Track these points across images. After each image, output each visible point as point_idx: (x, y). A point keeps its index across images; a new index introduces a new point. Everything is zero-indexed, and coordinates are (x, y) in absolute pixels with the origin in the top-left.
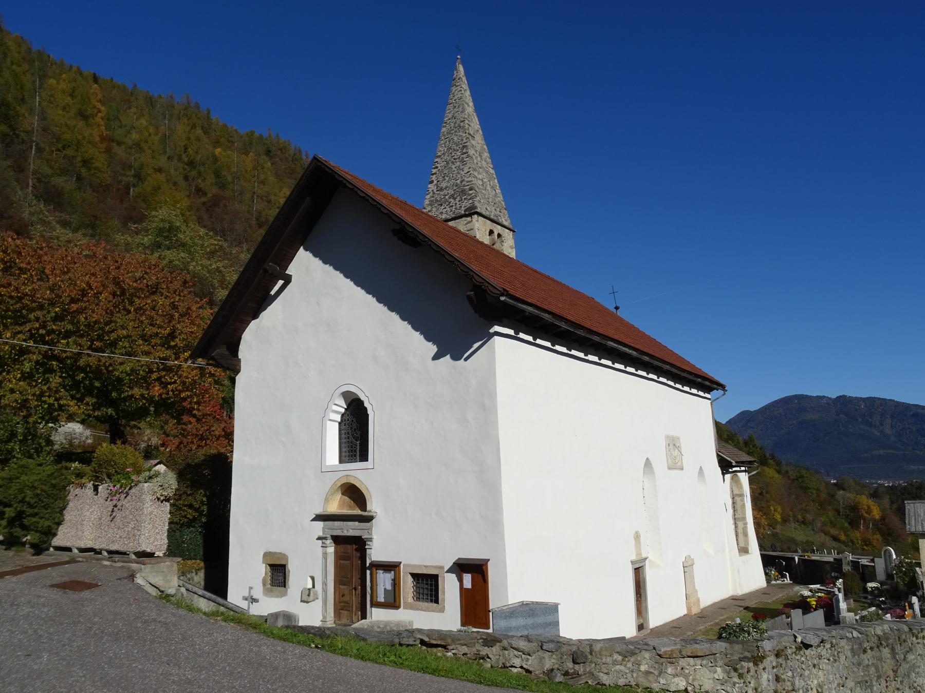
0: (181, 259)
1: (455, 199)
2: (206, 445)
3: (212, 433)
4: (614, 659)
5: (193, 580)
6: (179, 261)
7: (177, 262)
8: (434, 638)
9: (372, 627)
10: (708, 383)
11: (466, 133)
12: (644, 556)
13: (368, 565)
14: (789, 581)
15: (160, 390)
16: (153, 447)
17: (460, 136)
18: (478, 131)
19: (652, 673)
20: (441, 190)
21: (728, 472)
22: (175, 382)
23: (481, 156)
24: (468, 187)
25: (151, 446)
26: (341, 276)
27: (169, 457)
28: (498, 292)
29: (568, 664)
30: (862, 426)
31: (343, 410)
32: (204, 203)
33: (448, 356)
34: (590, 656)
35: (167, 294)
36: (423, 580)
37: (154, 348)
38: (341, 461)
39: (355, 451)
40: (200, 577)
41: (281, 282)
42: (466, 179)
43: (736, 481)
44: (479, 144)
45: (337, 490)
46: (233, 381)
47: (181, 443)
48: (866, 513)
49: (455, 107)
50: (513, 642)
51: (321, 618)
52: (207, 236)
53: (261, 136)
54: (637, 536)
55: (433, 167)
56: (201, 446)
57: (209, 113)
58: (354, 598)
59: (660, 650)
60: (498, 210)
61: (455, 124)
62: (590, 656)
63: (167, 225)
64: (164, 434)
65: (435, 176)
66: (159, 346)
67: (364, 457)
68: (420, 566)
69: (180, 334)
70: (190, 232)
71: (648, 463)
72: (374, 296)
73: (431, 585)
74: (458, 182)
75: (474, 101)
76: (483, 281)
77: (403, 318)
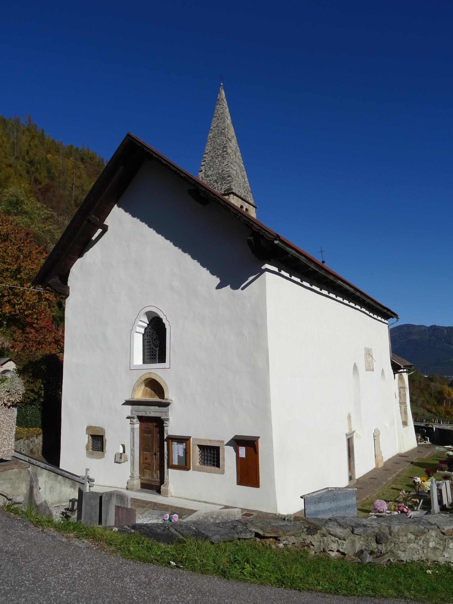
0: (24, 222)
1: (217, 183)
2: (42, 348)
3: (46, 340)
4: (409, 538)
5: (34, 442)
6: (23, 223)
7: (22, 224)
8: (268, 531)
9: (207, 518)
10: (389, 313)
11: (226, 137)
12: (353, 430)
13: (165, 438)
14: (429, 443)
15: (9, 308)
16: (5, 349)
17: (222, 139)
18: (233, 137)
19: (438, 549)
20: (208, 176)
21: (397, 373)
22: (21, 304)
23: (235, 155)
24: (227, 175)
25: (4, 348)
26: (146, 226)
27: (17, 356)
28: (273, 237)
29: (373, 544)
30: (444, 344)
31: (146, 325)
32: (40, 189)
33: (229, 286)
34: (389, 537)
35: (15, 241)
36: (207, 450)
37: (5, 279)
38: (144, 362)
39: (155, 355)
40: (39, 440)
41: (100, 231)
42: (226, 170)
43: (401, 378)
44: (234, 145)
45: (142, 383)
46: (61, 307)
47: (25, 346)
48: (448, 396)
49: (218, 119)
50: (331, 529)
51: (130, 475)
52: (42, 207)
53: (77, 148)
54: (349, 417)
55: (202, 160)
56: (39, 348)
57: (43, 131)
58: (154, 461)
59: (444, 529)
60: (246, 192)
61: (218, 131)
62: (389, 537)
63: (15, 199)
64: (13, 340)
65: (203, 167)
66: (9, 277)
67: (162, 359)
68: (205, 440)
69: (24, 270)
70: (31, 204)
71: (355, 367)
72: (171, 241)
73: (214, 454)
74: (220, 171)
75: (231, 116)
76: (261, 229)
77: (194, 257)
